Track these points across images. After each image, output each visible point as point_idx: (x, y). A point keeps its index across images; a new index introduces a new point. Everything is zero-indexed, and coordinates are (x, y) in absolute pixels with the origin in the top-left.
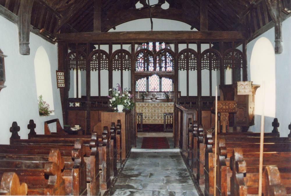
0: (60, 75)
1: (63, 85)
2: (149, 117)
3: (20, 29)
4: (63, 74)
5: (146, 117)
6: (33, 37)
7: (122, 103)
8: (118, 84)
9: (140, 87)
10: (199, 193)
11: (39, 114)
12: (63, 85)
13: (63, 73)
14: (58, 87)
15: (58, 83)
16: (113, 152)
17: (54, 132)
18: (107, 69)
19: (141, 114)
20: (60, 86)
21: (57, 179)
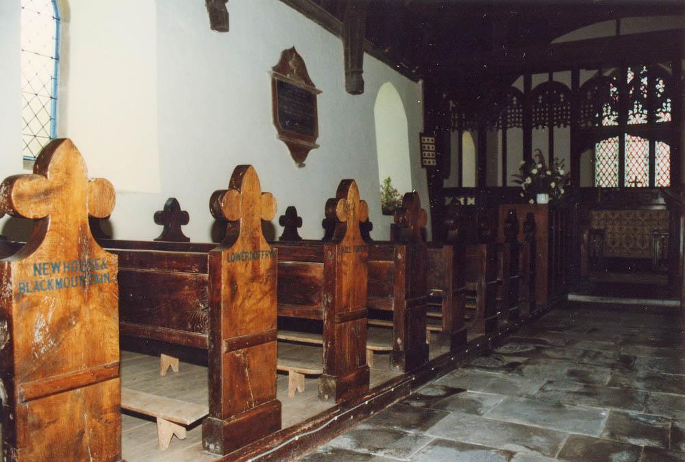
0: (426, 141)
1: (432, 163)
2: (621, 244)
3: (346, 45)
4: (432, 140)
5: (614, 243)
6: (371, 64)
7: (547, 190)
8: (539, 150)
9: (604, 178)
10: (463, 410)
11: (381, 211)
12: (432, 163)
13: (433, 139)
14: (423, 166)
15: (422, 158)
16: (348, 197)
17: (386, 240)
18: (521, 125)
19: (601, 233)
20: (427, 164)
21: (650, 424)
